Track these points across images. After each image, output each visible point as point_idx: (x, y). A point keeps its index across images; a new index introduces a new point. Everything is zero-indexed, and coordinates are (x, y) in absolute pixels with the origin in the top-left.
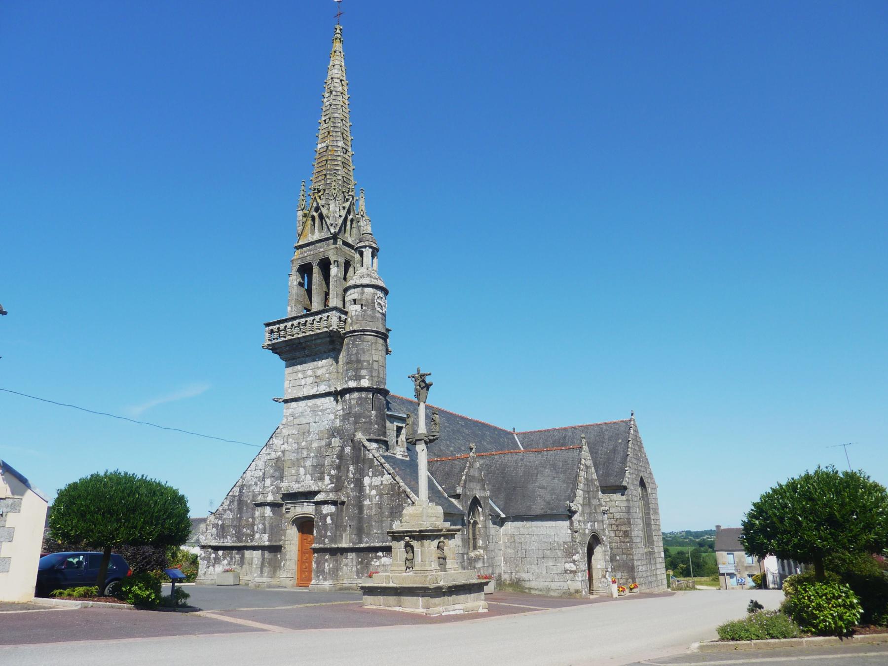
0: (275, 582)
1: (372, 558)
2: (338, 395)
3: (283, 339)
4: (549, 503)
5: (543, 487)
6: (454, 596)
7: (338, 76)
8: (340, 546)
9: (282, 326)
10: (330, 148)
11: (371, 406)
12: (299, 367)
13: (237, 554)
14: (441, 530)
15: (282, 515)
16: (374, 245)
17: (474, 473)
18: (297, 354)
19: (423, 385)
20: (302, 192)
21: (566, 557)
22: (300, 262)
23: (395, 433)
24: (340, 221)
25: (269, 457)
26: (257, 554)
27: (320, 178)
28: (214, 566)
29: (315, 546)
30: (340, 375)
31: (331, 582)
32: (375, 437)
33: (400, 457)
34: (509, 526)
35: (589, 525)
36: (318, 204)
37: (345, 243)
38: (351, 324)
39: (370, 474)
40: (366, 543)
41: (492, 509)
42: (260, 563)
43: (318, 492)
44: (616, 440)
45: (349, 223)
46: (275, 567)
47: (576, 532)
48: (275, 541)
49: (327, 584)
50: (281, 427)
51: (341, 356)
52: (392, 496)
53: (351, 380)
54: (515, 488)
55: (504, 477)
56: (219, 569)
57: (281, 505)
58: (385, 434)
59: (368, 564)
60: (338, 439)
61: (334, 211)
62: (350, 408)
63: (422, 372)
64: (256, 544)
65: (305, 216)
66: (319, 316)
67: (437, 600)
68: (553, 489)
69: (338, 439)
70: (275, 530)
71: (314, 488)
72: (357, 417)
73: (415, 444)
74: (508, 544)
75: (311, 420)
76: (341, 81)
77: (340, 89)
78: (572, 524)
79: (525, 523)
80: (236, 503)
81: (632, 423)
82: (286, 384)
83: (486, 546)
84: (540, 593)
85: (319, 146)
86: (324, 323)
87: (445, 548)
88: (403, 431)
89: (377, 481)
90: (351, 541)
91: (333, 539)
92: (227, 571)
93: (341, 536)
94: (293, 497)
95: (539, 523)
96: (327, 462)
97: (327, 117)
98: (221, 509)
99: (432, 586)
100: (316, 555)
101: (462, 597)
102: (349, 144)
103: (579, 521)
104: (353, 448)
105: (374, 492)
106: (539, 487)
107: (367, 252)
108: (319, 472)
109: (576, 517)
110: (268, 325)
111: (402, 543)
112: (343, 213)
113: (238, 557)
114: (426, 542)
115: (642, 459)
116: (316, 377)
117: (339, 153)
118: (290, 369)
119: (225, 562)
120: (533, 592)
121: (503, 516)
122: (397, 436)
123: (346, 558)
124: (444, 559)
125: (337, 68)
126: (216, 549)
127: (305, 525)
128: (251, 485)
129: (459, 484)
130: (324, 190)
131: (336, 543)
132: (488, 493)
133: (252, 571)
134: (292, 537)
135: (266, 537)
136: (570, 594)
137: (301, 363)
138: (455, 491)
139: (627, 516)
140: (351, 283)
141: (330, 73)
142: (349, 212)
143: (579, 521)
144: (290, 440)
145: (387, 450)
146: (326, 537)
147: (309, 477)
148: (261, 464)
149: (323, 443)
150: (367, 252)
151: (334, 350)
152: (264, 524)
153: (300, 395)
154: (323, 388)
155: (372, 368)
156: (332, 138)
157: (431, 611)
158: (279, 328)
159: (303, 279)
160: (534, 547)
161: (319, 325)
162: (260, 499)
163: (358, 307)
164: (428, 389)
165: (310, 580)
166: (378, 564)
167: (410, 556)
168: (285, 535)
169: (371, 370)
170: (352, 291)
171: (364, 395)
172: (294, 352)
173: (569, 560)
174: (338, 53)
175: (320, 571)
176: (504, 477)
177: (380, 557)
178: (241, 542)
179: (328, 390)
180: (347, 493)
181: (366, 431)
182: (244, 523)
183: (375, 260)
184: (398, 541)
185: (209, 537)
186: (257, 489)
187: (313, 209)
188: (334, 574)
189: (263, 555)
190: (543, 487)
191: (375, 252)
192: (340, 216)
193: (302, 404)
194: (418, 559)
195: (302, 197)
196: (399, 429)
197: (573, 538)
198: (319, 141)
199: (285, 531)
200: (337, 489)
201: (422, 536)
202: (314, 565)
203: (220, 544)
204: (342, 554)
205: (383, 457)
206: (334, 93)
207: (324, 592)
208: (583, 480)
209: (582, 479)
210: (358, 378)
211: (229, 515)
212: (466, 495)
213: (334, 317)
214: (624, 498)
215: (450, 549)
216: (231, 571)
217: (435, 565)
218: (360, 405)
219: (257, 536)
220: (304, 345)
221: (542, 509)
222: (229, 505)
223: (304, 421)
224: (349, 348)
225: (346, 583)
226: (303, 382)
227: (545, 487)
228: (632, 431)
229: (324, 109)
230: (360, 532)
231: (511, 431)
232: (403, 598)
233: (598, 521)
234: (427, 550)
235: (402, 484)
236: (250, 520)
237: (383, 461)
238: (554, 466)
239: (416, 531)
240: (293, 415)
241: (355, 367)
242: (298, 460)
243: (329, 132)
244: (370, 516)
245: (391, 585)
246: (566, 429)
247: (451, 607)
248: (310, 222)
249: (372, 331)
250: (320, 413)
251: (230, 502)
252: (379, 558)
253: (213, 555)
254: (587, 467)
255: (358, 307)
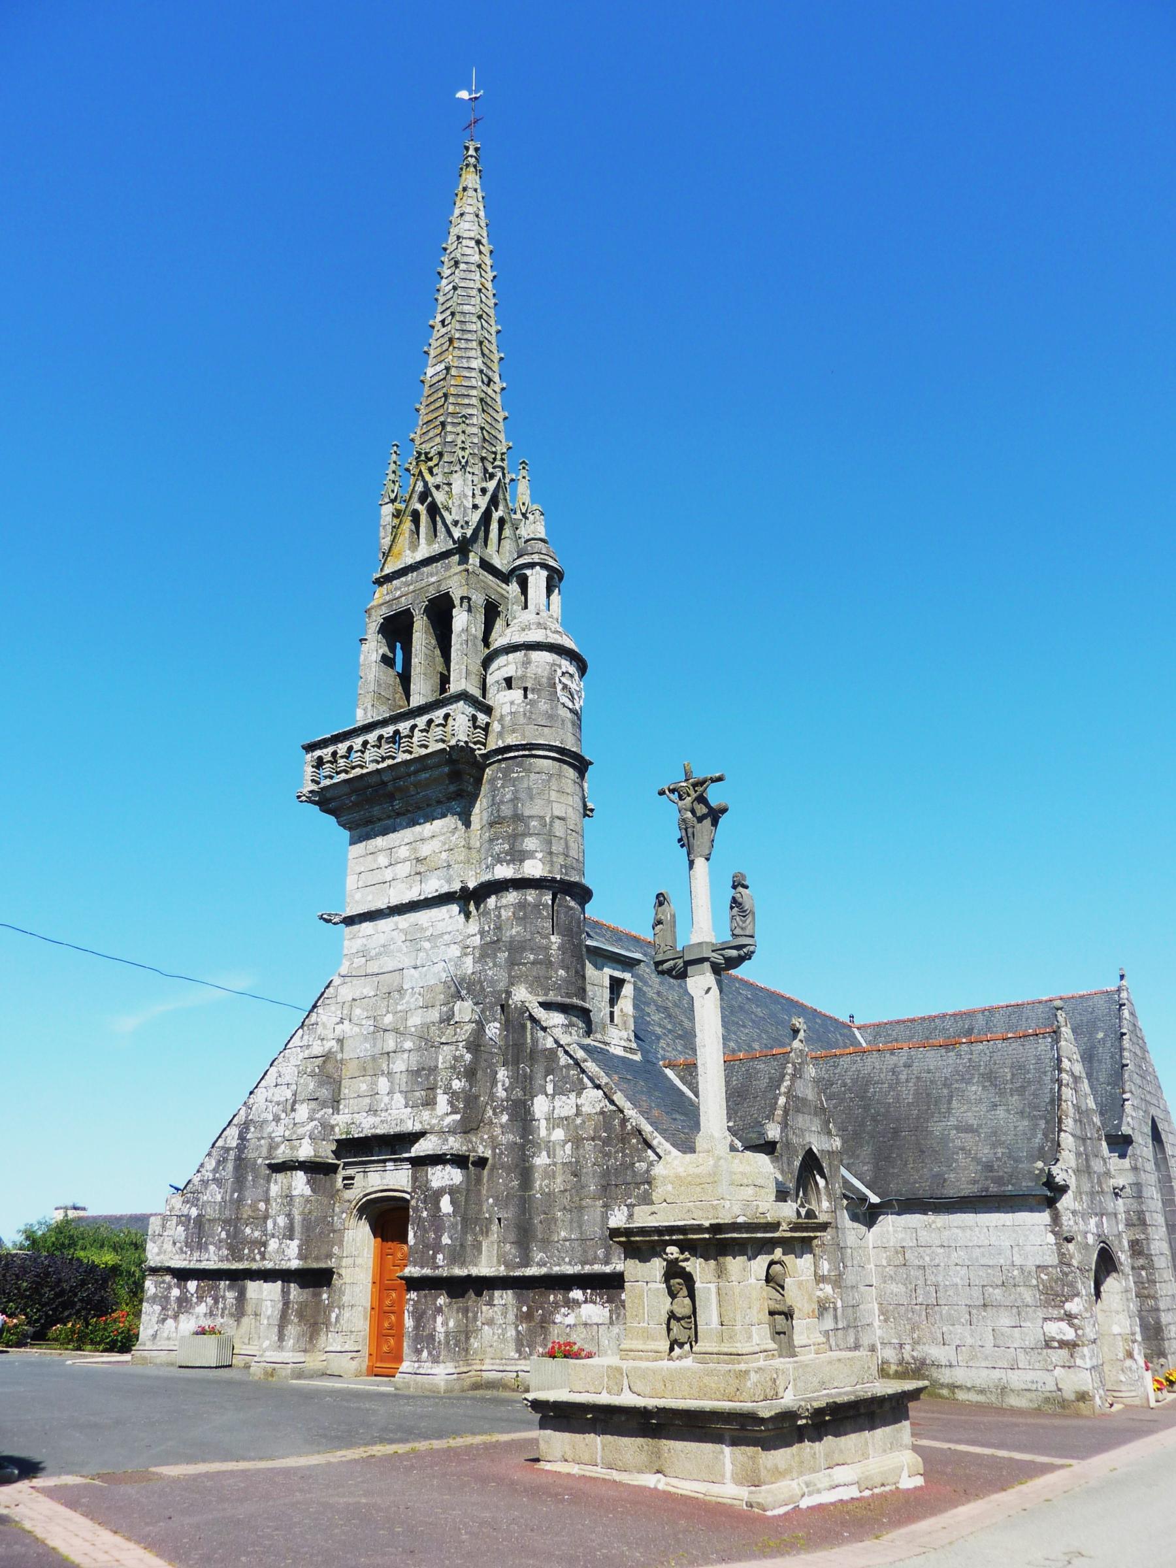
0: (314, 1361)
1: (556, 1305)
2: (469, 898)
3: (343, 776)
4: (989, 1167)
5: (969, 1129)
6: (829, 1440)
7: (472, 234)
8: (475, 1271)
9: (342, 748)
10: (453, 372)
11: (548, 925)
12: (380, 842)
13: (230, 1288)
14: (775, 1226)
15: (334, 1195)
16: (552, 563)
17: (806, 1091)
18: (376, 811)
19: (701, 810)
20: (393, 467)
21: (1046, 1304)
22: (385, 611)
23: (607, 994)
24: (475, 517)
25: (307, 1053)
26: (273, 1289)
27: (431, 434)
28: (176, 1317)
29: (412, 1271)
30: (474, 853)
31: (450, 1367)
32: (559, 999)
33: (619, 1052)
34: (889, 1224)
35: (1093, 1221)
36: (426, 484)
37: (486, 565)
38: (500, 735)
39: (550, 1089)
40: (542, 1264)
41: (846, 1182)
42: (277, 1314)
43: (421, 1134)
44: (1091, 1034)
45: (494, 526)
46: (314, 1323)
47: (1069, 1240)
48: (317, 1259)
49: (441, 1373)
50: (337, 981)
51: (476, 810)
52: (607, 1142)
53: (500, 861)
54: (896, 1132)
55: (866, 1108)
56: (187, 1325)
57: (333, 1169)
58: (582, 992)
59: (545, 1323)
60: (468, 1004)
61: (462, 497)
62: (498, 928)
63: (698, 775)
64: (269, 1265)
65: (397, 514)
66: (426, 718)
67: (781, 1457)
68: (995, 1133)
69: (468, 1004)
70: (317, 1231)
71: (410, 1126)
72: (516, 949)
73: (683, 975)
74: (890, 1270)
75: (407, 962)
76: (478, 242)
77: (476, 258)
78: (1056, 1219)
79: (930, 1217)
80: (230, 1166)
81: (1124, 995)
82: (351, 882)
83: (840, 1275)
84: (981, 1398)
85: (430, 371)
86: (437, 732)
87: (788, 1282)
88: (628, 990)
89: (565, 1106)
90: (502, 1259)
91: (457, 1255)
92: (203, 1332)
93: (478, 1247)
94: (362, 1148)
95: (968, 1218)
96: (444, 1058)
97: (448, 312)
98: (196, 1180)
99: (766, 1411)
100: (413, 1295)
101: (851, 1441)
102: (495, 367)
103: (1074, 1213)
104: (507, 1025)
105: (559, 1134)
106: (957, 1128)
107: (537, 579)
108: (423, 1084)
109: (1066, 1202)
110: (310, 748)
111: (657, 1266)
112: (483, 502)
113: (231, 1296)
114: (735, 1264)
115: (1147, 1075)
116: (418, 860)
117: (474, 382)
118: (360, 848)
119: (202, 1309)
120: (961, 1396)
121: (875, 1199)
122: (612, 1002)
123: (490, 1304)
124: (788, 1315)
125: (469, 220)
126: (183, 1275)
127: (387, 1218)
128: (265, 1121)
129: (770, 1117)
130: (441, 454)
131: (463, 1264)
132: (837, 1143)
133: (260, 1331)
134: (357, 1251)
135: (293, 1247)
136: (1063, 1404)
137: (384, 832)
138: (762, 1134)
139: (1135, 1207)
140: (499, 639)
141: (454, 231)
142: (494, 502)
143: (1074, 1213)
144: (357, 1012)
145: (589, 1032)
146: (438, 1247)
147: (399, 1099)
148: (288, 1069)
149: (434, 1015)
150: (537, 579)
151: (459, 795)
152: (289, 1215)
153: (382, 904)
154: (434, 886)
155: (551, 834)
156: (457, 353)
157: (763, 1495)
158: (334, 754)
159: (392, 649)
160: (958, 1277)
161: (425, 741)
162: (282, 1153)
163: (517, 694)
164: (715, 823)
165: (399, 1359)
166: (570, 1320)
167: (682, 1306)
168: (341, 1245)
169: (548, 839)
170: (501, 660)
171: (531, 896)
172: (368, 804)
173: (1055, 1313)
174: (471, 193)
175: (425, 1339)
176: (866, 1108)
177: (577, 1303)
178: (241, 1260)
179: (445, 889)
180: (493, 1138)
181: (538, 983)
182: (246, 1212)
183: (555, 597)
184: (644, 1259)
185: (168, 1246)
186: (279, 1131)
187: (416, 497)
188: (461, 1343)
189: (285, 1293)
190: (969, 1129)
191: (555, 579)
192: (475, 507)
193: (385, 925)
194: (708, 1317)
195: (392, 476)
196: (616, 985)
197: (1061, 1255)
198: (431, 361)
199: (340, 1232)
200: (469, 1125)
201: (719, 1242)
202: (409, 1323)
203: (193, 1265)
204: (479, 1294)
205: (584, 1047)
206: (462, 266)
207: (431, 1396)
208: (1071, 1111)
209: (1068, 1107)
210: (518, 856)
211: (214, 1194)
212: (788, 1144)
213: (461, 714)
214: (1126, 1163)
215: (800, 1284)
216: (213, 1331)
217: (761, 1337)
218: (522, 920)
219: (273, 1244)
220: (390, 787)
221: (975, 1182)
222: (215, 1171)
223: (389, 964)
224: (494, 789)
225: (489, 1369)
226: (388, 874)
227: (976, 1129)
228: (1126, 1013)
229: (441, 299)
230: (524, 1236)
231: (847, 1020)
232: (667, 1445)
233: (1107, 1214)
234: (733, 1290)
235: (631, 1112)
236: (262, 1206)
237: (580, 1054)
238: (990, 1078)
239: (699, 1229)
240: (364, 953)
241: (511, 829)
242: (374, 1058)
243: (451, 340)
244: (549, 1196)
245: (627, 1399)
246: (970, 1014)
247: (822, 1479)
248: (408, 525)
249: (551, 748)
250: (427, 945)
251: (219, 1163)
252: (573, 1304)
253: (176, 1292)
254: (1076, 1079)
255: (517, 694)
